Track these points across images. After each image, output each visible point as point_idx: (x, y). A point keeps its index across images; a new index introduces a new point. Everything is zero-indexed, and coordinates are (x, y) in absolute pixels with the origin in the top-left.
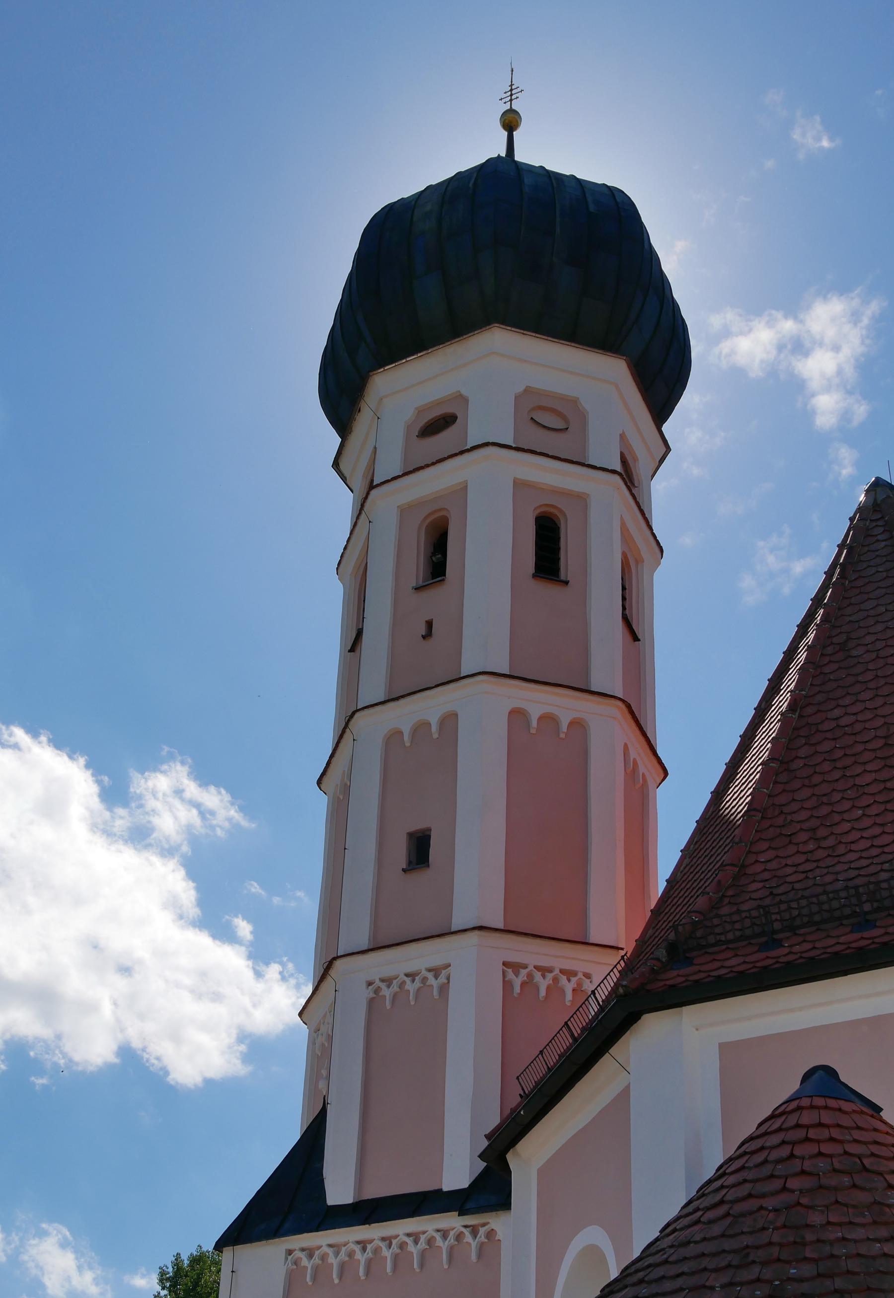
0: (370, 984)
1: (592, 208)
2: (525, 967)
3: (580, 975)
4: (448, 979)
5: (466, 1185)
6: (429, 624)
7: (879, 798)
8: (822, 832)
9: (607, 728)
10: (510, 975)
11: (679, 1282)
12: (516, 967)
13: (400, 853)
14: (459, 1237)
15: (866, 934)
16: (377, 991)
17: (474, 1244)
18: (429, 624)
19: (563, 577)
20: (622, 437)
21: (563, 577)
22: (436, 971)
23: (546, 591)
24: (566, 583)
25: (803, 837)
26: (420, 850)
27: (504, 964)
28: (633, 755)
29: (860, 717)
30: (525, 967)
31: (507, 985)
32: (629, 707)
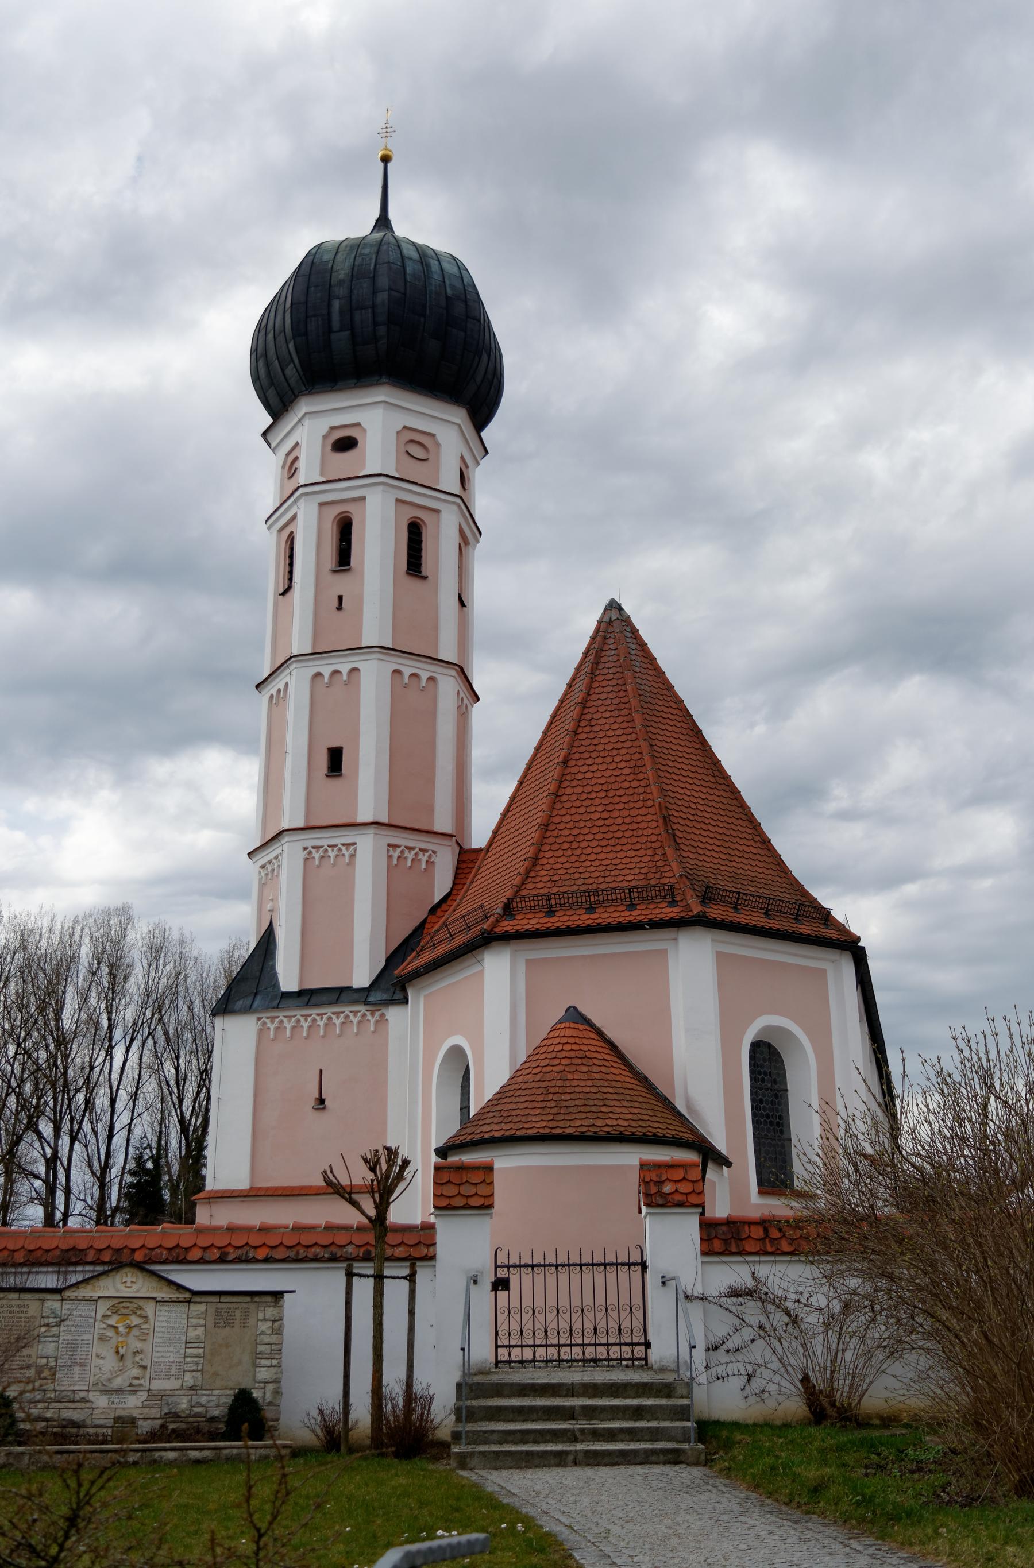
0: (305, 849)
1: (449, 292)
2: (399, 847)
3: (430, 852)
4: (355, 850)
5: (367, 985)
6: (340, 598)
7: (615, 689)
8: (575, 845)
9: (448, 685)
10: (391, 853)
11: (526, 1098)
12: (394, 846)
13: (323, 761)
14: (364, 1015)
15: (592, 916)
16: (310, 853)
17: (373, 1021)
18: (340, 598)
19: (423, 574)
20: (462, 458)
21: (423, 574)
22: (347, 845)
23: (414, 584)
24: (425, 578)
25: (566, 846)
26: (335, 760)
27: (389, 845)
28: (462, 694)
29: (600, 709)
30: (399, 847)
31: (390, 857)
32: (462, 669)
